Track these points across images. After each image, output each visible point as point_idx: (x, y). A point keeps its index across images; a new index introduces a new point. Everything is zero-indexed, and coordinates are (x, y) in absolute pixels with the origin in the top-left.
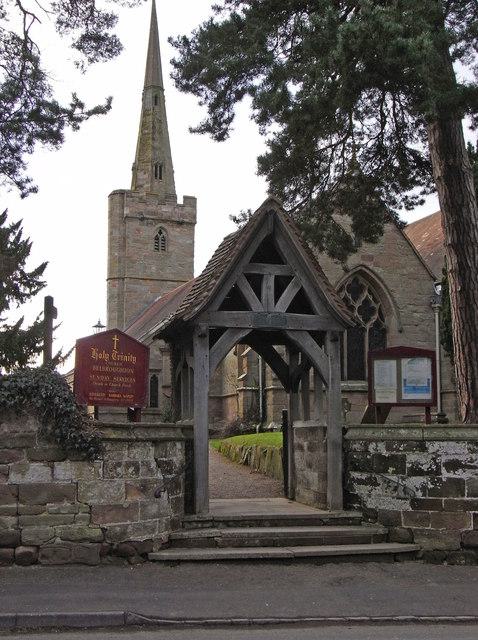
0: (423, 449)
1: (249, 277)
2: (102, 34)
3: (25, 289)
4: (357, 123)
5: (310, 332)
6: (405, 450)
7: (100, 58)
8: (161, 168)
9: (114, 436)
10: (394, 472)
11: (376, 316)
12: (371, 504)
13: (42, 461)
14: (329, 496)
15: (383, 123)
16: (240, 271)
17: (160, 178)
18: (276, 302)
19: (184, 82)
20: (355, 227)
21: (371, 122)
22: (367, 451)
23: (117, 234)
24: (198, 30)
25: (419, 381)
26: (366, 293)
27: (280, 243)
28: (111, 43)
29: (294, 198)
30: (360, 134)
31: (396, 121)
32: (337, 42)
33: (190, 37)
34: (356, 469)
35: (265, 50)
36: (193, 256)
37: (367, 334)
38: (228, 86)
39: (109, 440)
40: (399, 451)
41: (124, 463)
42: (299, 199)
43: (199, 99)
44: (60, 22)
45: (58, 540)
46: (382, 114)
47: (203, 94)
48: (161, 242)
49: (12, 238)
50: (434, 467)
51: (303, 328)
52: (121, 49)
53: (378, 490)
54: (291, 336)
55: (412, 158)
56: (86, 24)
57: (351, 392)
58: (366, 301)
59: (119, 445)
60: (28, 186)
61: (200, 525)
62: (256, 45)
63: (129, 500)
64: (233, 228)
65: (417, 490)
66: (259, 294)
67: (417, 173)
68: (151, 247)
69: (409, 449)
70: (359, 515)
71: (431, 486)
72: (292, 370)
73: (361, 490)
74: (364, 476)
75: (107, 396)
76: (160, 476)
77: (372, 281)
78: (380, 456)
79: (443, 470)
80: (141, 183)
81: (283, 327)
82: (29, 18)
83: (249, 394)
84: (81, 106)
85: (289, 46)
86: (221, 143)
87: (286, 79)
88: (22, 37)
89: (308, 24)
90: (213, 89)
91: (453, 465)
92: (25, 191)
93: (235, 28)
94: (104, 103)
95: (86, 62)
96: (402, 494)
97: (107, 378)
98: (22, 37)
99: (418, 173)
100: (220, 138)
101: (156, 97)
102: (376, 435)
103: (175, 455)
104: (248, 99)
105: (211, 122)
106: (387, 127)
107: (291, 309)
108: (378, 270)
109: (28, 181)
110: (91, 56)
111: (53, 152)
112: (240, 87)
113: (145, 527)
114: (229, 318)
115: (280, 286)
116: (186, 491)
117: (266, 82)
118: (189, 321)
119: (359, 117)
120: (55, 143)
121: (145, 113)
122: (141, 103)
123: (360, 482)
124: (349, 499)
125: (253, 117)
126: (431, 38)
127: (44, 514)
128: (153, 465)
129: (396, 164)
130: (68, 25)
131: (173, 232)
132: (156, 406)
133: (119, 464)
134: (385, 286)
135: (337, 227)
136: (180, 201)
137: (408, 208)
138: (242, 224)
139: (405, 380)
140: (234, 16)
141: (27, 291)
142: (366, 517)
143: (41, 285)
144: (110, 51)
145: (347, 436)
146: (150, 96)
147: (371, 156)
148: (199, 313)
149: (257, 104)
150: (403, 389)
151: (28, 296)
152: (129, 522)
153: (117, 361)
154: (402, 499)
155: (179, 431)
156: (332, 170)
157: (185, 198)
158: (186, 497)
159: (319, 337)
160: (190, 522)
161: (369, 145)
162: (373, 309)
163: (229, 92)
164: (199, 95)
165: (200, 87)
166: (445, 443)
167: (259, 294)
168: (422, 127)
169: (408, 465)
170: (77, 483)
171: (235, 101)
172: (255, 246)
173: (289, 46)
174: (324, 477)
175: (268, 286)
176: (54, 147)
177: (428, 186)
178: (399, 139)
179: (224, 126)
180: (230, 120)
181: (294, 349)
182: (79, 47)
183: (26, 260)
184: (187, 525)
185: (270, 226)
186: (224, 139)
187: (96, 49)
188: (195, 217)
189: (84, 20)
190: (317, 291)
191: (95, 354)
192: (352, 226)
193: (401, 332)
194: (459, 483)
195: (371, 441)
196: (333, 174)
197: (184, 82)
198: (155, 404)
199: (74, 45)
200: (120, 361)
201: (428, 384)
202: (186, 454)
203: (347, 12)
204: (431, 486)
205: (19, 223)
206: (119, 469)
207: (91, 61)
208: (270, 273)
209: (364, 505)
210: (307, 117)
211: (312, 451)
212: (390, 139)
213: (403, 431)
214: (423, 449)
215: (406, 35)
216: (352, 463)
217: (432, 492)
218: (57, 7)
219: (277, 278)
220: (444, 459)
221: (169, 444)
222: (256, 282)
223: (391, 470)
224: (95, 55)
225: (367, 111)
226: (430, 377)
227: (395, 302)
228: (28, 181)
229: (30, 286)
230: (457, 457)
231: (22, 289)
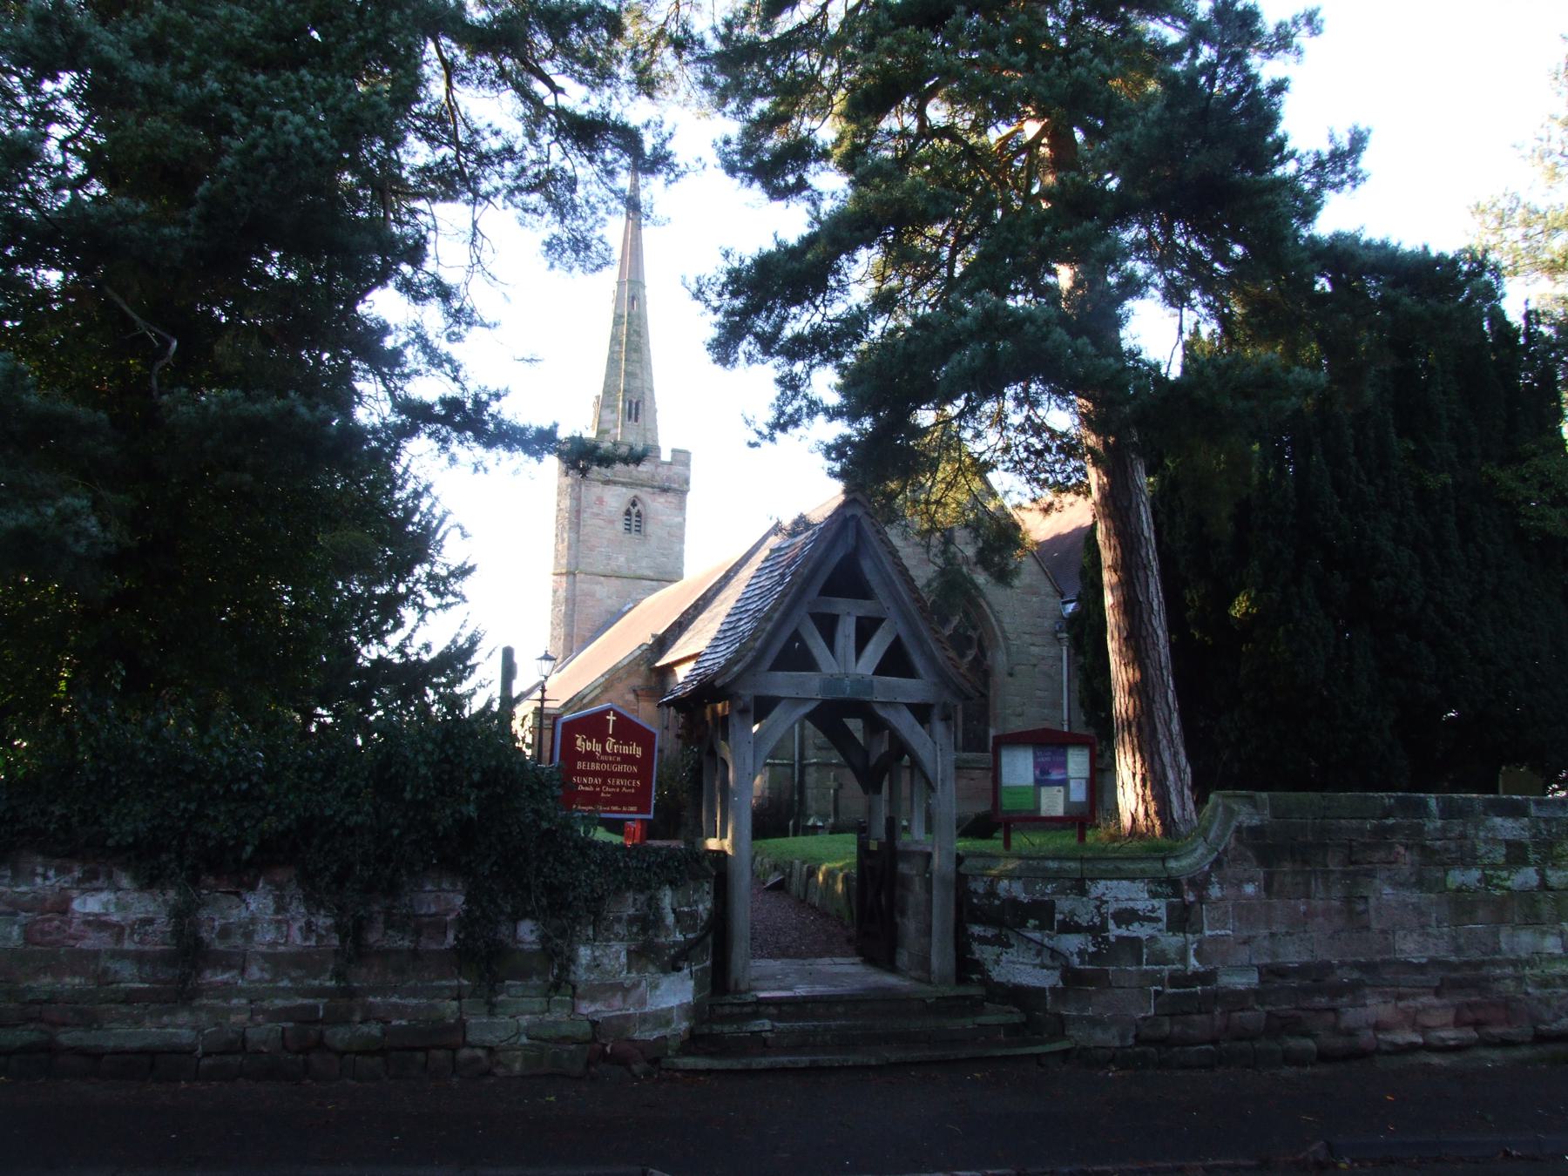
0: (1083, 892)
5: (906, 704)
6: (1054, 893)
8: (637, 404)
10: (1035, 928)
12: (998, 974)
14: (935, 962)
17: (636, 420)
27: (866, 565)
34: (978, 921)
45: (524, 1040)
48: (634, 518)
51: (899, 700)
66: (831, 645)
68: (620, 526)
69: (1062, 891)
73: (984, 953)
74: (990, 933)
78: (1013, 902)
79: (1111, 925)
81: (867, 698)
91: (1127, 916)
107: (880, 670)
114: (783, 683)
115: (865, 632)
123: (984, 940)
124: (966, 966)
131: (656, 505)
134: (988, 603)
145: (962, 869)
148: (740, 675)
153: (613, 754)
154: (1048, 968)
157: (675, 452)
159: (922, 712)
166: (1115, 882)
167: (831, 645)
175: (846, 631)
181: (876, 725)
185: (851, 540)
188: (687, 482)
190: (920, 641)
191: (581, 744)
194: (1135, 942)
200: (618, 754)
204: (1091, 949)
208: (848, 614)
217: (1094, 957)
219: (859, 619)
220: (1112, 907)
222: (827, 626)
223: (1031, 922)
227: (1003, 631)
229: (442, 595)
230: (1131, 904)
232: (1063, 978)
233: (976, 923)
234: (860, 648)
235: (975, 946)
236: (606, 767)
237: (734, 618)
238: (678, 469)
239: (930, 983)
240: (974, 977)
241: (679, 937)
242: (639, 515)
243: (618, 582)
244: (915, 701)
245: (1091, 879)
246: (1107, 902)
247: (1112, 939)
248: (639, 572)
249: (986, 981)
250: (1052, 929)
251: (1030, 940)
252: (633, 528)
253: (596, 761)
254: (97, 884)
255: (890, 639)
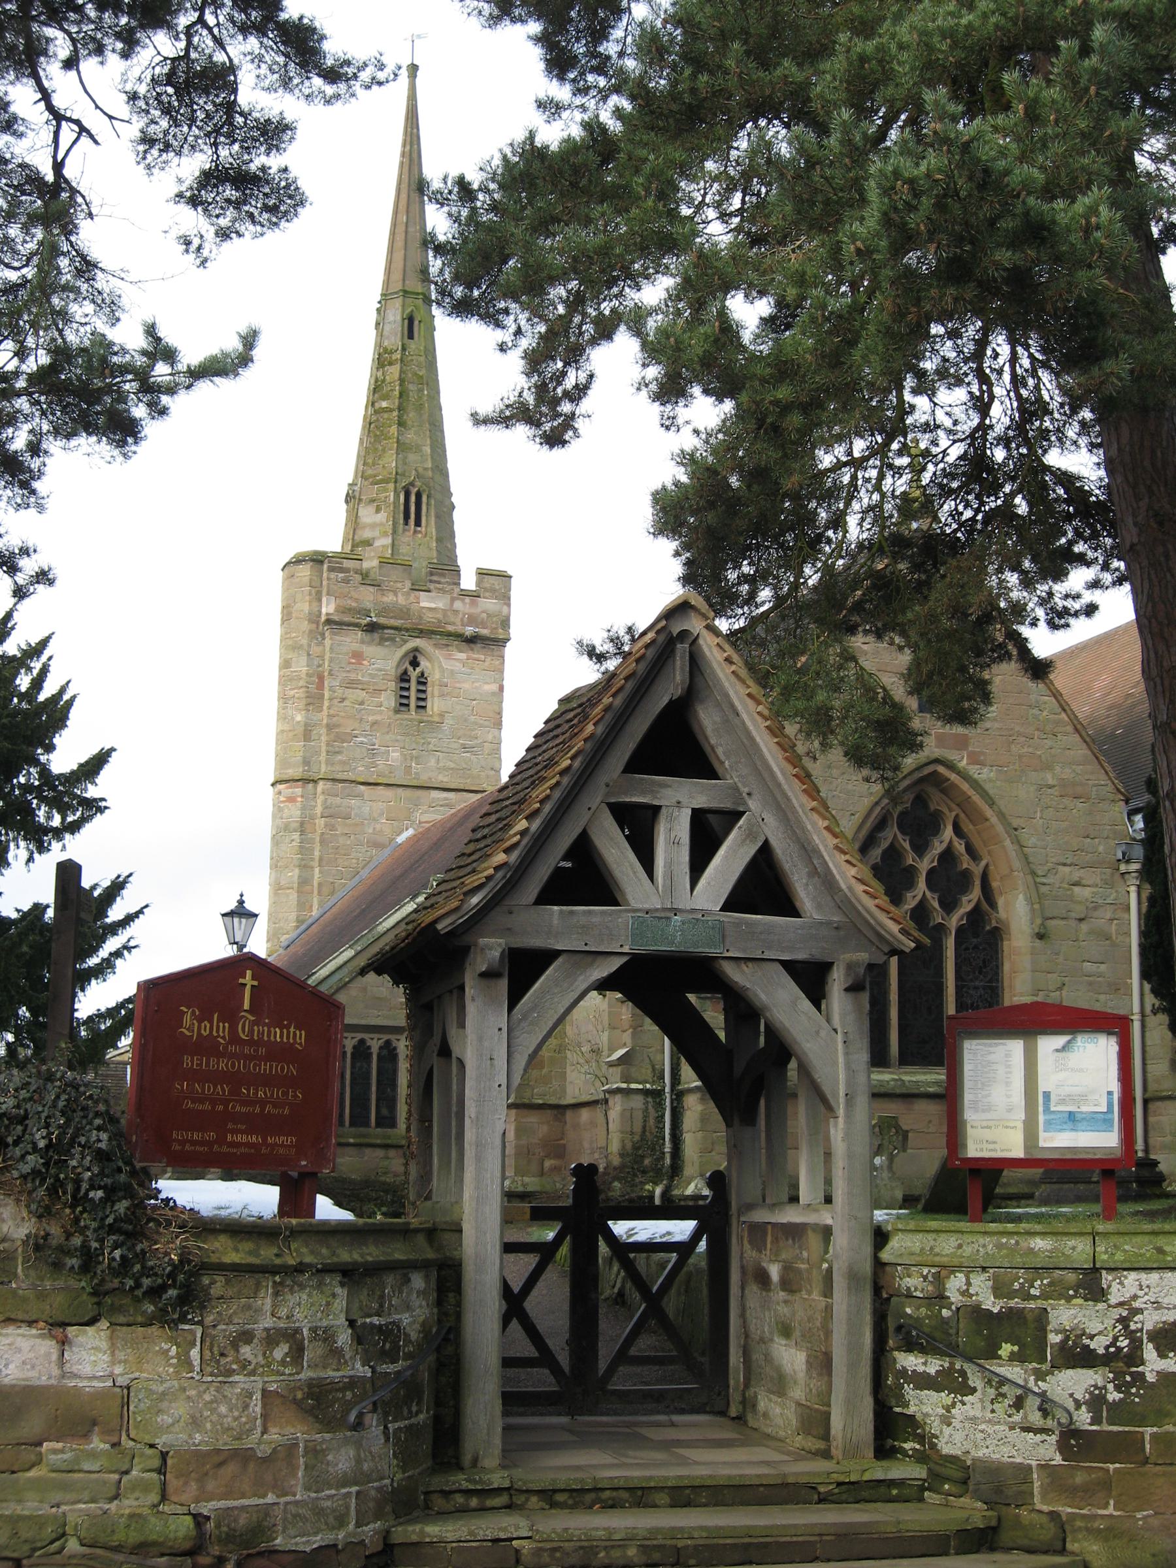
0: (1096, 1293)
1: (624, 814)
2: (253, 167)
3: (49, 817)
4: (922, 402)
5: (787, 965)
7: (248, 228)
8: (419, 496)
9: (232, 1257)
10: (1013, 1357)
11: (976, 893)
13: (31, 1323)
15: (982, 405)
16: (595, 799)
17: (418, 523)
18: (694, 882)
19: (459, 291)
20: (918, 680)
21: (953, 398)
22: (940, 1298)
23: (301, 666)
24: (497, 162)
25: (1083, 1098)
26: (948, 833)
27: (707, 719)
28: (276, 190)
29: (753, 594)
30: (927, 428)
31: (1019, 397)
32: (863, 201)
33: (475, 178)
34: (910, 1346)
35: (673, 215)
36: (498, 724)
37: (950, 943)
38: (576, 303)
39: (221, 1268)
40: (1029, 1297)
41: (260, 1334)
42: (765, 594)
43: (500, 335)
44: (147, 140)
45: (73, 1545)
46: (983, 379)
47: (509, 321)
49: (24, 682)
50: (1124, 1343)
52: (302, 203)
53: (972, 1406)
54: (737, 975)
55: (1061, 491)
56: (215, 145)
57: (909, 1096)
58: (948, 856)
59: (249, 1280)
60: (28, 566)
61: (474, 1502)
62: (650, 203)
63: (274, 1435)
64: (588, 674)
65: (1078, 1405)
67: (1076, 530)
68: (388, 699)
69: (1057, 1292)
70: (917, 1472)
71: (1113, 1396)
72: (739, 1067)
74: (933, 1366)
75: (221, 1140)
76: (361, 1370)
77: (964, 804)
78: (978, 1314)
79: (1149, 1352)
80: (367, 534)
81: (712, 951)
82: (68, 133)
83: (638, 1102)
84: (169, 355)
85: (736, 201)
86: (557, 452)
87: (727, 287)
88: (50, 178)
89: (784, 150)
90: (537, 313)
92: (21, 578)
93: (593, 158)
94: (233, 344)
95: (210, 233)
96: (1036, 1418)
97: (223, 1090)
98: (50, 178)
99: (1079, 535)
100: (554, 440)
101: (411, 320)
102: (968, 1250)
103: (408, 1308)
104: (625, 345)
105: (530, 398)
106: (996, 410)
108: (983, 774)
109: (25, 551)
110: (224, 222)
111: (116, 465)
112: (606, 308)
113: (319, 1512)
116: (438, 1403)
117: (674, 296)
118: (451, 934)
119: (925, 387)
120: (121, 444)
121: (382, 360)
122: (373, 333)
123: (924, 1382)
125: (643, 384)
126: (1114, 204)
127: (32, 1473)
128: (344, 1338)
129: (1022, 506)
130: (167, 147)
132: (392, 1123)
133: (246, 1337)
135: (868, 686)
136: (468, 581)
137: (1053, 626)
138: (611, 664)
139: (1047, 1095)
140: (593, 127)
141: (56, 821)
142: (935, 1481)
143: (94, 807)
144: (273, 210)
146: (395, 315)
147: (955, 485)
149: (652, 351)
150: (1041, 1118)
151: (58, 833)
152: (270, 1498)
153: (251, 1042)
154: (1037, 1431)
155: (421, 1239)
156: (852, 521)
157: (482, 574)
158: (437, 1420)
160: (446, 1494)
161: (951, 459)
162: (966, 875)
163: (577, 319)
164: (499, 325)
165: (502, 305)
166: (1154, 1276)
167: (647, 860)
168: (1087, 414)
169: (1054, 1338)
170: (128, 1388)
171: (594, 342)
172: (639, 727)
173: (736, 201)
174: (822, 1364)
176: (116, 452)
177: (1105, 567)
178: (1027, 442)
179: (566, 407)
180: (581, 391)
182: (194, 202)
183: (57, 740)
184: (438, 1502)
186: (564, 443)
187: (237, 204)
188: (505, 623)
189: (208, 135)
190: (808, 852)
191: (190, 1024)
192: (906, 677)
193: (1041, 936)
195: (953, 1269)
196: (856, 530)
197: (459, 291)
198: (388, 1121)
199: (180, 195)
200: (259, 1043)
201: (1110, 1105)
202: (439, 1303)
203: (888, 122)
204: (1113, 1396)
205: (44, 643)
206: (246, 1351)
207: (224, 234)
209: (933, 1446)
210: (783, 393)
211: (791, 1291)
212: (1004, 441)
213: (1039, 1243)
214: (1096, 1293)
215: (1049, 192)
216: (899, 1328)
217: (1117, 1412)
218: (141, 104)
219: (698, 817)
220: (1149, 1320)
221: (390, 1280)
223: (1006, 1349)
224: (234, 221)
225: (948, 376)
226: (1115, 1086)
228: (25, 551)
229: (63, 810)
231: (41, 815)
232: (1063, 1446)
233: (909, 1350)
234: (698, 865)
235: (909, 1391)
236: (240, 1065)
237: (493, 818)
238: (488, 604)
239: (826, 1454)
240: (907, 1446)
241: (361, 1370)
242: (422, 681)
243: (389, 793)
244: (801, 956)
245: (1110, 1270)
246: (1140, 1311)
247: (1151, 1378)
248: (424, 779)
249: (928, 1455)
250: (1043, 1360)
251: (1003, 1381)
252: (413, 702)
253: (220, 1055)
254: (415, 1514)
255: (749, 852)
